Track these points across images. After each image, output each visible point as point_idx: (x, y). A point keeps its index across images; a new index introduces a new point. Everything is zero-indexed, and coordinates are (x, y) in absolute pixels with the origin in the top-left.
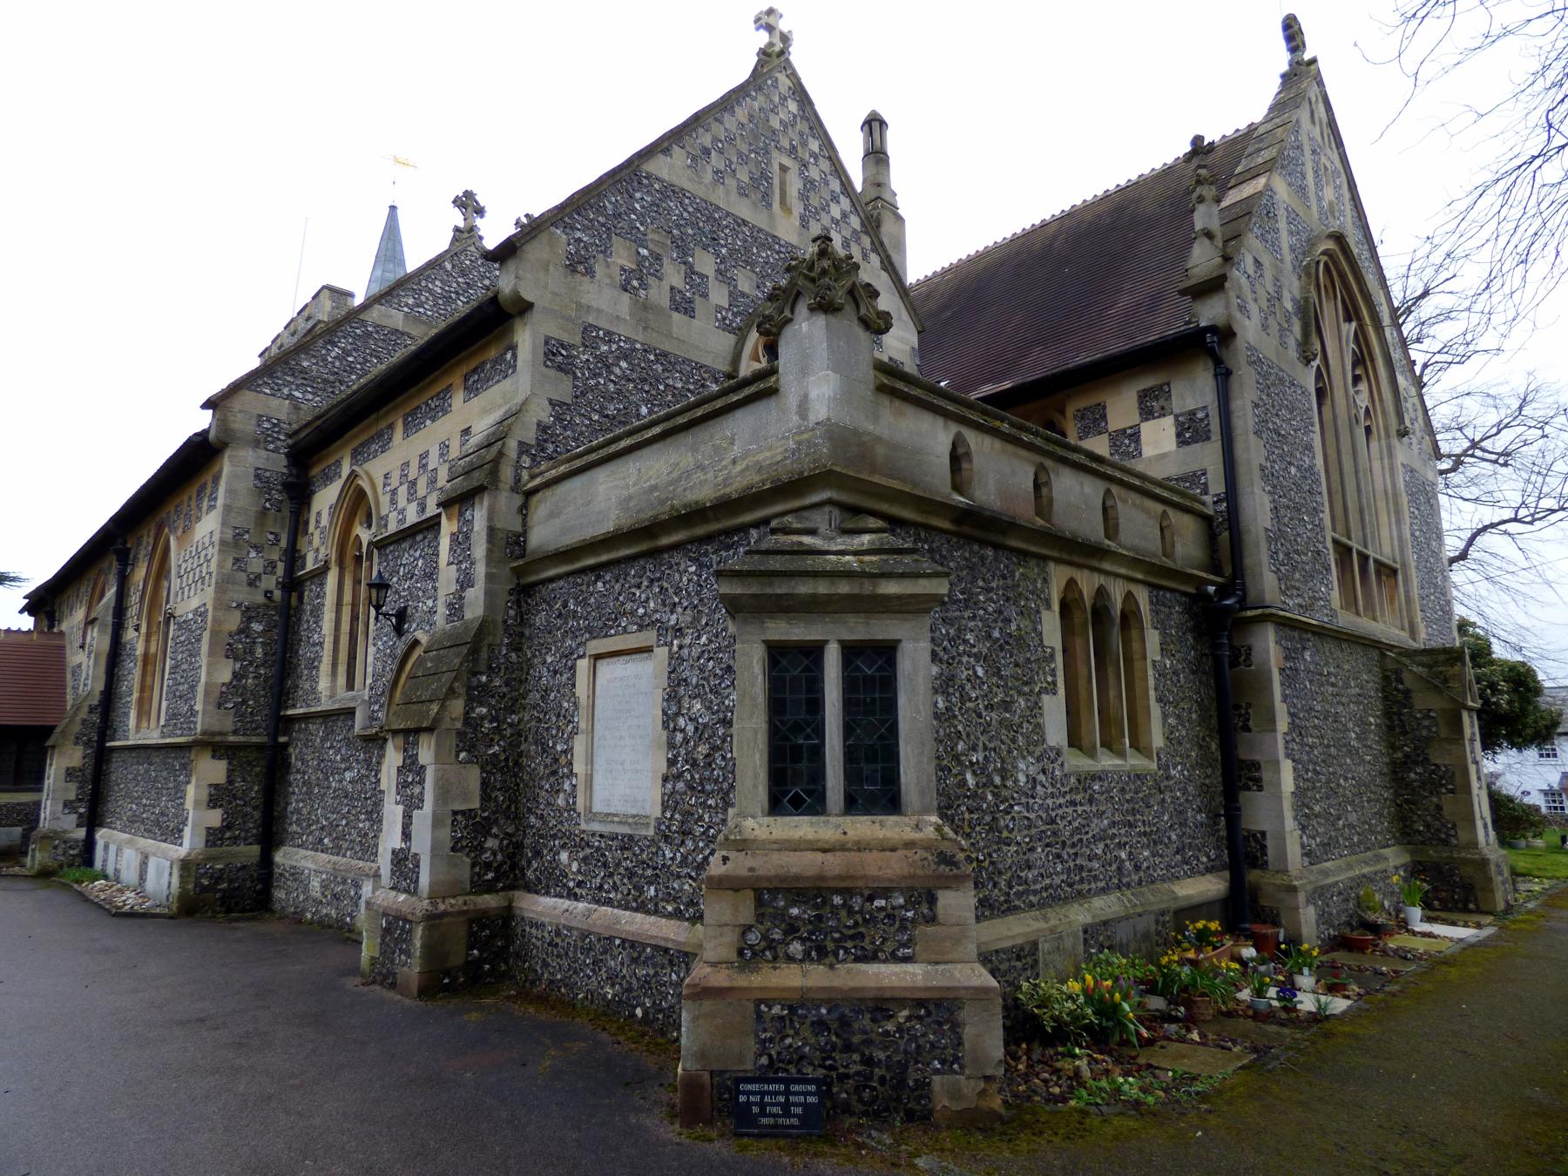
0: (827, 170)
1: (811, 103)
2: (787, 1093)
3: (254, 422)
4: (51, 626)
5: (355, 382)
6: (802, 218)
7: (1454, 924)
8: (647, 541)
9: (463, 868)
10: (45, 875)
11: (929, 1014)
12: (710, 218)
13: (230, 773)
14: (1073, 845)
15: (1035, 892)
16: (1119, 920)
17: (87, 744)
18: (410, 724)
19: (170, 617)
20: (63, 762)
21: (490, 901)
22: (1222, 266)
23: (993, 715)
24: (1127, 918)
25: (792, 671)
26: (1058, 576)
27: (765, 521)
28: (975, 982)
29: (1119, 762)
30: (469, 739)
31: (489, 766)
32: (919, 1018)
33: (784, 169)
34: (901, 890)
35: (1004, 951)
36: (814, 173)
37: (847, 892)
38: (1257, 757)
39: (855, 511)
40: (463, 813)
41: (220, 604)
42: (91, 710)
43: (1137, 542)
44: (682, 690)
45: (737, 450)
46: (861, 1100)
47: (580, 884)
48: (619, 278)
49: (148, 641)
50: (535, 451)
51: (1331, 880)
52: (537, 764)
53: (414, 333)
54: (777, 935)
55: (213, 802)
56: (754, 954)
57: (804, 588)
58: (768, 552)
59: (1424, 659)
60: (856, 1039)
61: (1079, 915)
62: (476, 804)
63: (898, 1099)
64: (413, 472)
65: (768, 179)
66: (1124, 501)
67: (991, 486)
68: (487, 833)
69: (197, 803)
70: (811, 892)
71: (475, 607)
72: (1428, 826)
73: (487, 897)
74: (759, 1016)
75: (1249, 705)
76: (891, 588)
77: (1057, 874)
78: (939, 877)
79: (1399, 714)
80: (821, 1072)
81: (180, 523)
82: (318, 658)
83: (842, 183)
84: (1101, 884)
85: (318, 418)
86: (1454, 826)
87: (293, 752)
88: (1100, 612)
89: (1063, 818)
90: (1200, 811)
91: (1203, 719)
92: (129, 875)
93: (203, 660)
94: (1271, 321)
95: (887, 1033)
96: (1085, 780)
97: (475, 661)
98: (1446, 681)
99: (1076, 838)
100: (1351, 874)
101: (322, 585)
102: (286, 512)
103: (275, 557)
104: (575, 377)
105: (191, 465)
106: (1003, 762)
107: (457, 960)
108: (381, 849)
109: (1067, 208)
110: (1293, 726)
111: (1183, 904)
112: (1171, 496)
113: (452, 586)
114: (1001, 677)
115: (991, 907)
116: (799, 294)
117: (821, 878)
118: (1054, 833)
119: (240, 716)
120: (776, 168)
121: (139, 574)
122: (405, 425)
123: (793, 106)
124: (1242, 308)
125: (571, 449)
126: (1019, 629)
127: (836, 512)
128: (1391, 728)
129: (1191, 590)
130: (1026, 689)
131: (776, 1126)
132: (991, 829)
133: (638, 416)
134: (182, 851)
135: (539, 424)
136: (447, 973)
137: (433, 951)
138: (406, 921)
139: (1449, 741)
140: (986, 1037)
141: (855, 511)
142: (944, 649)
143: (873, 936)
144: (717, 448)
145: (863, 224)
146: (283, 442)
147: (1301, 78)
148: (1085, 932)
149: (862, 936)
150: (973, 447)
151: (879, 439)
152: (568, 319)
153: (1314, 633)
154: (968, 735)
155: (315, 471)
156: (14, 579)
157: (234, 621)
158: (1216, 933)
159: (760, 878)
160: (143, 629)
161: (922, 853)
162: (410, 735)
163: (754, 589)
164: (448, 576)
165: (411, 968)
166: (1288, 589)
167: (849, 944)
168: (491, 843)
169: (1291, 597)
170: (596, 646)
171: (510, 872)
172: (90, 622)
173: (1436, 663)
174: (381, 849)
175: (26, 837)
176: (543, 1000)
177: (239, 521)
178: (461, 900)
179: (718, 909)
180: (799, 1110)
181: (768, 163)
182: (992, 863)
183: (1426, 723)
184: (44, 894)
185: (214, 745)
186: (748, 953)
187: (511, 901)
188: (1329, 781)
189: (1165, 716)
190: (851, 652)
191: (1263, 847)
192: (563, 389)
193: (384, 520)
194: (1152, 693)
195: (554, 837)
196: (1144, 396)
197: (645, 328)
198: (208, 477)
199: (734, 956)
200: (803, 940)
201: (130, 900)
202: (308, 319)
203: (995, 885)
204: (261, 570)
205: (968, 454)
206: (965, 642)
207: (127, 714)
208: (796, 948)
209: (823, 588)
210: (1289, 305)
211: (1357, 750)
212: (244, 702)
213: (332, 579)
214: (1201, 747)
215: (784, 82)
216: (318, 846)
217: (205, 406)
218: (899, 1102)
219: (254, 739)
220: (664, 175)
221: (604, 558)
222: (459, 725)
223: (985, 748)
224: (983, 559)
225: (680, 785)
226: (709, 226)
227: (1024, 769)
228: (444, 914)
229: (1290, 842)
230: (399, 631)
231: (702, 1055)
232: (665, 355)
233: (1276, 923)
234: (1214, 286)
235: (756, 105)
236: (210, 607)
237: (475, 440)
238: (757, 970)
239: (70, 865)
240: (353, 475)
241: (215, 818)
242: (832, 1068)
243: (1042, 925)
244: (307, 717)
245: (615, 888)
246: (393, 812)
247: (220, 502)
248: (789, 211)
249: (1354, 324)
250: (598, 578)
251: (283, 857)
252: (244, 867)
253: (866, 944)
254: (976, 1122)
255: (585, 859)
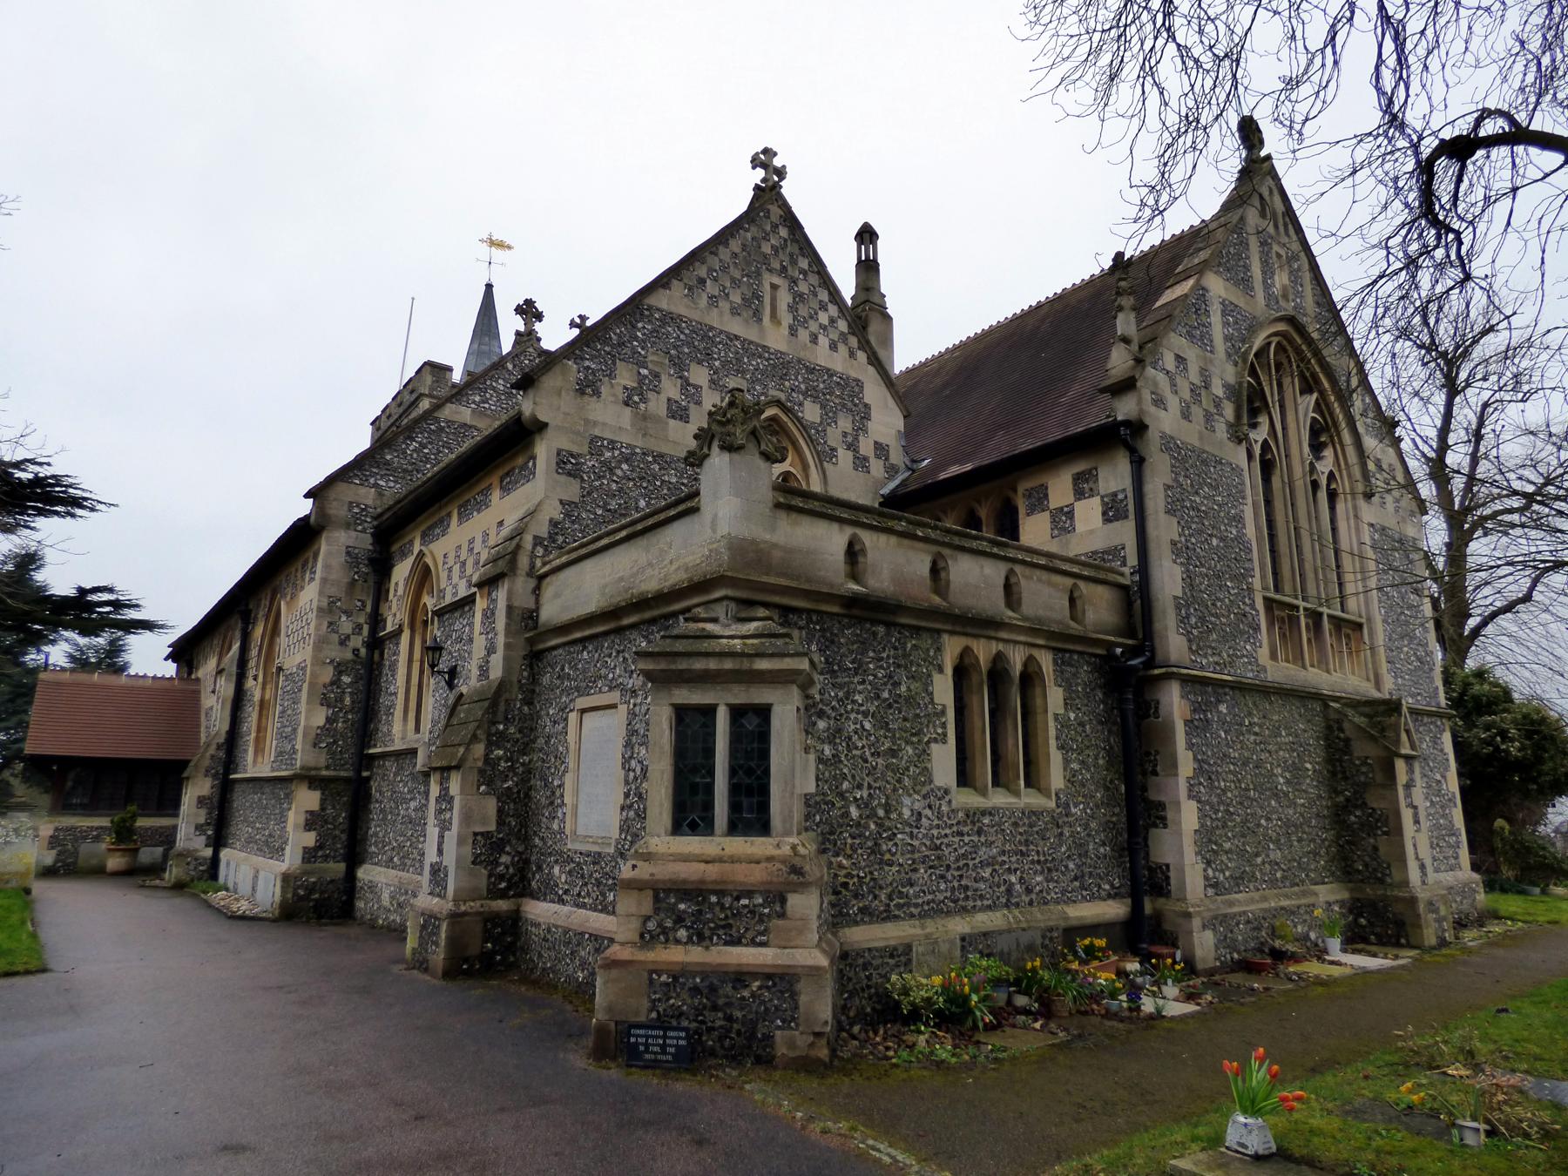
0: (816, 283)
1: (801, 227)
2: (665, 1037)
3: (346, 508)
4: (190, 673)
5: (430, 470)
6: (791, 327)
7: (1375, 955)
8: (614, 621)
9: (482, 878)
10: (179, 887)
11: (775, 985)
12: (705, 337)
13: (323, 801)
14: (959, 869)
15: (916, 905)
16: (1000, 932)
17: (215, 776)
18: (444, 763)
19: (280, 669)
20: (197, 790)
21: (502, 905)
22: (1134, 368)
23: (880, 761)
24: (1009, 931)
25: (692, 727)
26: (952, 648)
27: (688, 609)
28: (810, 962)
29: (1013, 800)
30: (488, 776)
31: (504, 797)
32: (768, 988)
33: (774, 287)
34: (760, 892)
35: (877, 949)
36: (803, 287)
37: (721, 893)
38: (1162, 798)
39: (750, 603)
40: (482, 834)
41: (318, 661)
42: (219, 747)
43: (1041, 612)
44: (634, 739)
45: (672, 553)
46: (722, 1046)
47: (566, 892)
48: (622, 396)
49: (264, 689)
50: (546, 543)
51: (1235, 909)
52: (541, 796)
53: (479, 425)
54: (669, 923)
55: (309, 826)
56: (652, 937)
57: (699, 665)
58: (677, 637)
59: (1367, 710)
60: (721, 1002)
61: (959, 926)
62: (493, 828)
63: (750, 1047)
64: (464, 554)
65: (759, 298)
66: (1029, 578)
67: (886, 574)
68: (502, 851)
69: (296, 826)
70: (694, 892)
71: (496, 672)
72: (1366, 865)
73: (500, 902)
74: (651, 981)
75: (1157, 752)
76: (763, 665)
77: (940, 891)
78: (789, 883)
79: (1340, 761)
80: (694, 1025)
81: (289, 591)
82: (393, 706)
83: (830, 293)
84: (986, 903)
85: (399, 502)
86: (1389, 867)
87: (374, 785)
88: (998, 674)
89: (948, 845)
90: (1104, 844)
91: (1110, 764)
92: (245, 888)
93: (303, 706)
94: (1195, 409)
95: (743, 998)
96: (973, 816)
97: (495, 713)
98: (1383, 730)
99: (961, 863)
100: (1265, 905)
101: (397, 644)
102: (371, 580)
103: (362, 620)
104: (582, 480)
105: (295, 545)
106: (887, 798)
107: (474, 949)
108: (424, 864)
109: (1087, 277)
110: (1199, 771)
111: (1074, 923)
112: (1095, 569)
113: (483, 651)
114: (889, 730)
115: (871, 915)
116: (713, 436)
117: (702, 882)
118: (939, 858)
119: (332, 754)
120: (767, 287)
121: (258, 631)
122: (459, 514)
123: (784, 232)
124: (1159, 402)
125: (572, 542)
126: (909, 689)
127: (733, 605)
128: (1333, 774)
129: (1099, 651)
130: (915, 739)
131: (655, 1061)
132: (873, 852)
133: (637, 509)
134: (283, 867)
135: (551, 520)
136: (466, 960)
137: (454, 943)
138: (436, 918)
139: (1383, 786)
140: (820, 1005)
141: (750, 603)
142: (833, 708)
143: (740, 926)
144: (661, 550)
145: (850, 326)
146: (369, 524)
147: (1257, 173)
148: (963, 939)
149: (730, 926)
150: (867, 544)
151: (775, 546)
152: (578, 433)
153: (1232, 688)
154: (853, 777)
155: (395, 548)
156: (162, 627)
157: (327, 675)
158: (1101, 949)
159: (657, 881)
160: (260, 679)
161: (778, 865)
162: (445, 770)
163: (663, 666)
164: (480, 643)
165: (438, 956)
166: (1197, 644)
167: (721, 932)
168: (505, 859)
169: (1205, 656)
170: (583, 702)
171: (520, 884)
172: (220, 672)
173: (1376, 714)
174: (424, 864)
175: (165, 856)
176: (535, 983)
177: (333, 591)
178: (478, 903)
179: (629, 904)
180: (672, 1050)
181: (760, 284)
182: (873, 879)
183: (1364, 769)
184: (179, 902)
185: (310, 778)
186: (647, 936)
187: (519, 906)
188: (1245, 822)
189: (1066, 762)
190: (737, 712)
191: (1168, 878)
192: (572, 490)
193: (442, 592)
194: (1053, 743)
195: (550, 854)
196: (1078, 478)
197: (644, 435)
198: (310, 554)
199: (637, 939)
200: (688, 928)
201: (243, 907)
202: (412, 392)
203: (875, 897)
204: (349, 631)
205: (863, 551)
206: (854, 702)
207: (246, 751)
208: (682, 934)
209: (713, 665)
210: (1218, 391)
211: (1286, 794)
212: (335, 742)
213: (405, 638)
214: (1107, 789)
215: (775, 211)
216: (389, 864)
217: (307, 496)
218: (749, 1050)
219: (343, 774)
220: (664, 305)
221: (587, 633)
222: (480, 764)
223: (870, 787)
224: (875, 634)
225: (632, 813)
226: (703, 344)
227: (908, 805)
228: (465, 914)
229: (1192, 876)
230: (451, 685)
231: (610, 1009)
232: (661, 456)
233: (1175, 946)
234: (1126, 386)
235: (749, 235)
236: (308, 663)
237: (505, 532)
238: (653, 949)
239: (200, 879)
240: (421, 554)
241: (310, 839)
242: (702, 1022)
243: (919, 931)
244: (384, 755)
245: (588, 894)
246: (433, 832)
247: (318, 575)
248: (779, 323)
249: (1315, 395)
250: (585, 648)
251: (365, 873)
252: (332, 881)
253: (733, 932)
254: (805, 1065)
255: (570, 872)
